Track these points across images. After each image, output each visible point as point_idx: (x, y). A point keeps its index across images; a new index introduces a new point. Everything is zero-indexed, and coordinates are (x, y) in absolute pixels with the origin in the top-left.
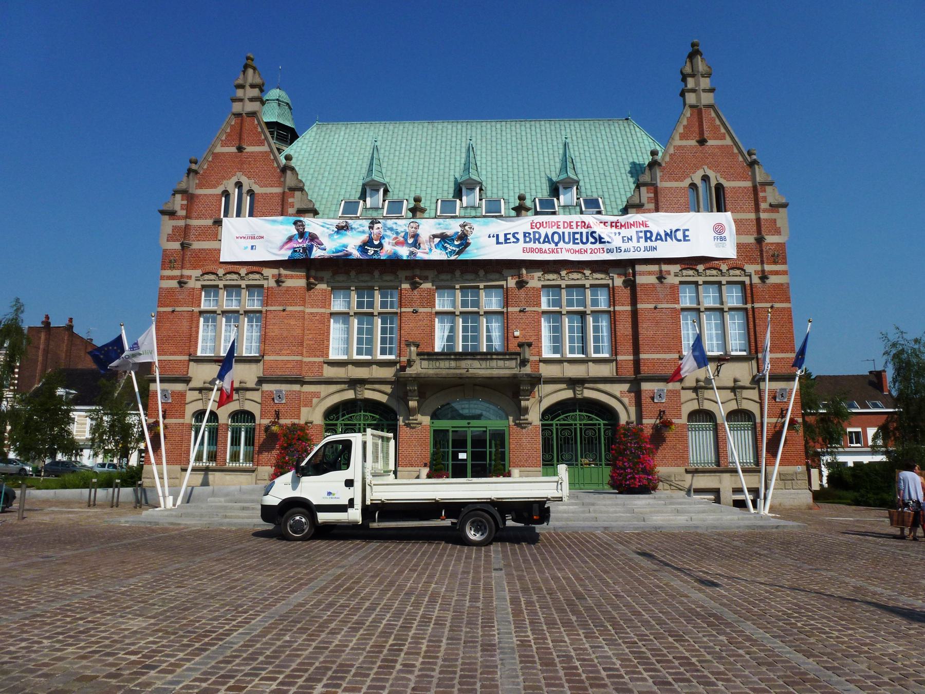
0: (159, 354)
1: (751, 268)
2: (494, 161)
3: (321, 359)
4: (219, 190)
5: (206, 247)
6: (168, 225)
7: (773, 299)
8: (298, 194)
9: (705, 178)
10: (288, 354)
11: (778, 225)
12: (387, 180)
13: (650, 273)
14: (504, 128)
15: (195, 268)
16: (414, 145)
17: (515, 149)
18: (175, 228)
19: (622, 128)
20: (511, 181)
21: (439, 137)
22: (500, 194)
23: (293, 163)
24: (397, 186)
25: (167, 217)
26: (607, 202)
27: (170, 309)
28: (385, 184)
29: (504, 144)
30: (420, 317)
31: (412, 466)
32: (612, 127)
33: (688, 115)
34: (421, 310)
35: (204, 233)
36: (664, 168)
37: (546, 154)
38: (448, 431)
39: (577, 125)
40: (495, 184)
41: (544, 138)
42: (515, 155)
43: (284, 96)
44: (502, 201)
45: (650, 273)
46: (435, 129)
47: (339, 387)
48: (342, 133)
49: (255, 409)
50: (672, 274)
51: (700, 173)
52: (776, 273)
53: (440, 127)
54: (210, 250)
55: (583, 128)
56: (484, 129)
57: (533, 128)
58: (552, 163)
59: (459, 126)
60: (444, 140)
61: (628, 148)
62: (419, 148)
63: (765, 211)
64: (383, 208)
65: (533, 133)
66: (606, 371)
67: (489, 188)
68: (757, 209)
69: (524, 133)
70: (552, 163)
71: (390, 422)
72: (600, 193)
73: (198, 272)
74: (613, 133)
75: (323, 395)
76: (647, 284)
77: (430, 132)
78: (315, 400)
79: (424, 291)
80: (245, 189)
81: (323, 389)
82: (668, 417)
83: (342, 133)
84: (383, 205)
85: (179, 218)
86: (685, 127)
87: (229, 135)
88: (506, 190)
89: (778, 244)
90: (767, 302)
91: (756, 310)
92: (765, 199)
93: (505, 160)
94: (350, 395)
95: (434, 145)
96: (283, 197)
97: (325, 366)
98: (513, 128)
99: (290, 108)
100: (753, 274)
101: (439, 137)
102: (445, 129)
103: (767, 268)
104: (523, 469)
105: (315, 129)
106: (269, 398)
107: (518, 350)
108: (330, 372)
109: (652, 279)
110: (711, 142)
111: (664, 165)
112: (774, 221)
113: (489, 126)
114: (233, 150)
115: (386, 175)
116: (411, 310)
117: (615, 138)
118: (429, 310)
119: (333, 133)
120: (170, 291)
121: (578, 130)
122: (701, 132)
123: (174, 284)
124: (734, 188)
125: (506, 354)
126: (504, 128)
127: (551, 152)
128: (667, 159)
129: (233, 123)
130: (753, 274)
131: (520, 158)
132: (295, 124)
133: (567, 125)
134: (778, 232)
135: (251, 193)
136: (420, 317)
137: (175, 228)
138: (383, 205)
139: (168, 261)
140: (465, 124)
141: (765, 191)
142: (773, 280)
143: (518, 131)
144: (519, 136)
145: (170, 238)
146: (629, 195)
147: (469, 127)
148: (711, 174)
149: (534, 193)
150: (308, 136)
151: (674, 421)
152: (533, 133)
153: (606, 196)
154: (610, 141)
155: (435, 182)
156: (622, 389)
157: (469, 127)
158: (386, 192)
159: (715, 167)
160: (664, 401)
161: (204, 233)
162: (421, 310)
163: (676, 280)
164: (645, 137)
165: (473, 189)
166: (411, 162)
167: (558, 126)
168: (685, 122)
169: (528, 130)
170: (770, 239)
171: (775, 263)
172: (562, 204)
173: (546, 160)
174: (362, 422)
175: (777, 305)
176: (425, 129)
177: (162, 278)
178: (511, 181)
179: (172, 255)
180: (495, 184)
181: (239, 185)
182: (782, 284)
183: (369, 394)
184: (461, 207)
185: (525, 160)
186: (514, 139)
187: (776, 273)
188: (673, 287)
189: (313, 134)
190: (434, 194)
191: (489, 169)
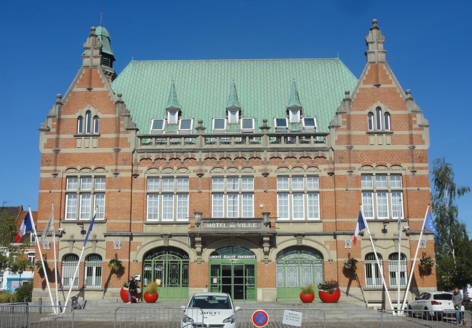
0: (231, 286)
1: (405, 165)
2: (249, 90)
3: (142, 222)
4: (76, 116)
5: (69, 152)
6: (44, 138)
7: (418, 184)
8: (127, 118)
9: (379, 109)
10: (122, 219)
11: (423, 138)
12: (180, 107)
13: (343, 169)
14: (255, 66)
15: (62, 165)
16: (197, 78)
17: (262, 82)
18: (49, 140)
19: (333, 66)
20: (259, 104)
21: (213, 73)
22: (252, 115)
23: (123, 99)
24: (187, 108)
25: (43, 133)
26: (320, 120)
27: (48, 191)
28: (180, 109)
29: (255, 78)
30: (203, 196)
31: (198, 287)
32: (326, 65)
33: (369, 68)
34: (203, 191)
35: (68, 143)
36: (353, 102)
37: (282, 86)
38: (220, 265)
39: (303, 63)
40: (249, 107)
41: (281, 73)
42: (262, 86)
43: (106, 33)
44: (253, 120)
45: (343, 169)
46: (210, 66)
47: (155, 238)
48: (150, 69)
49: (103, 253)
50: (357, 168)
51: (375, 106)
52: (422, 168)
53: (214, 64)
54: (72, 154)
55: (307, 66)
56: (242, 66)
57: (275, 66)
58: (286, 92)
59: (226, 64)
60: (216, 75)
61: (335, 81)
62: (200, 80)
63: (416, 129)
64: (178, 124)
65: (275, 69)
66: (318, 228)
67: (245, 110)
68: (410, 128)
69: (268, 70)
70: (286, 92)
71: (184, 260)
72: (316, 114)
73: (65, 168)
74: (327, 70)
75: (143, 244)
76: (341, 176)
77: (207, 68)
78: (138, 247)
79: (205, 179)
80: (93, 115)
81: (143, 240)
82: (353, 256)
83: (150, 69)
84: (178, 122)
85: (52, 133)
86: (367, 76)
87: (82, 80)
88: (256, 112)
89: (422, 150)
90: (415, 186)
91: (408, 191)
92: (415, 122)
93: (256, 90)
94: (161, 243)
95: (210, 78)
96: (118, 120)
97: (144, 225)
98: (262, 66)
99: (109, 40)
100: (407, 169)
101: (213, 73)
102: (217, 67)
103: (416, 165)
104: (265, 288)
105: (131, 65)
106: (110, 245)
107: (266, 216)
108: (149, 229)
109: (345, 173)
110: (382, 86)
111: (353, 100)
112: (421, 136)
113: (246, 64)
114: (84, 90)
115: (183, 104)
116: (197, 191)
117: (327, 73)
118: (208, 191)
119: (143, 69)
120: (47, 180)
121: (304, 68)
122: (377, 80)
123: (49, 175)
124: (396, 115)
125: (257, 220)
126: (255, 66)
127: (285, 84)
128: (355, 97)
129: (84, 72)
130: (407, 169)
131: (266, 88)
132: (114, 53)
133: (297, 64)
134: (423, 143)
135: (96, 117)
136: (203, 196)
137: (49, 140)
138: (178, 122)
139: (45, 161)
140: (230, 62)
141: (415, 117)
142: (419, 173)
143: (265, 68)
144: (265, 72)
145: (46, 146)
146: (339, 105)
147: (233, 64)
148: (381, 105)
149: (273, 114)
150: (127, 71)
151: (357, 259)
152: (275, 69)
153: (319, 116)
154: (324, 76)
155: (211, 105)
156: (326, 240)
157: (233, 64)
158: (180, 114)
159: (384, 101)
160: (350, 247)
161: (68, 143)
162: (203, 191)
163: (359, 173)
164: (347, 73)
165: (235, 112)
166: (195, 91)
167: (291, 64)
168: (367, 73)
169: (271, 67)
170: (418, 147)
171: (421, 162)
172: (291, 121)
173: (282, 90)
174: (167, 260)
175: (421, 188)
176: (204, 67)
177: (42, 171)
178: (259, 104)
179: (47, 157)
180: (249, 107)
181: (88, 112)
182: (425, 176)
183: (172, 243)
184: (228, 124)
185: (269, 90)
186: (262, 74)
187: (422, 168)
188: (357, 177)
189: (131, 69)
190: (211, 114)
191: (245, 96)
